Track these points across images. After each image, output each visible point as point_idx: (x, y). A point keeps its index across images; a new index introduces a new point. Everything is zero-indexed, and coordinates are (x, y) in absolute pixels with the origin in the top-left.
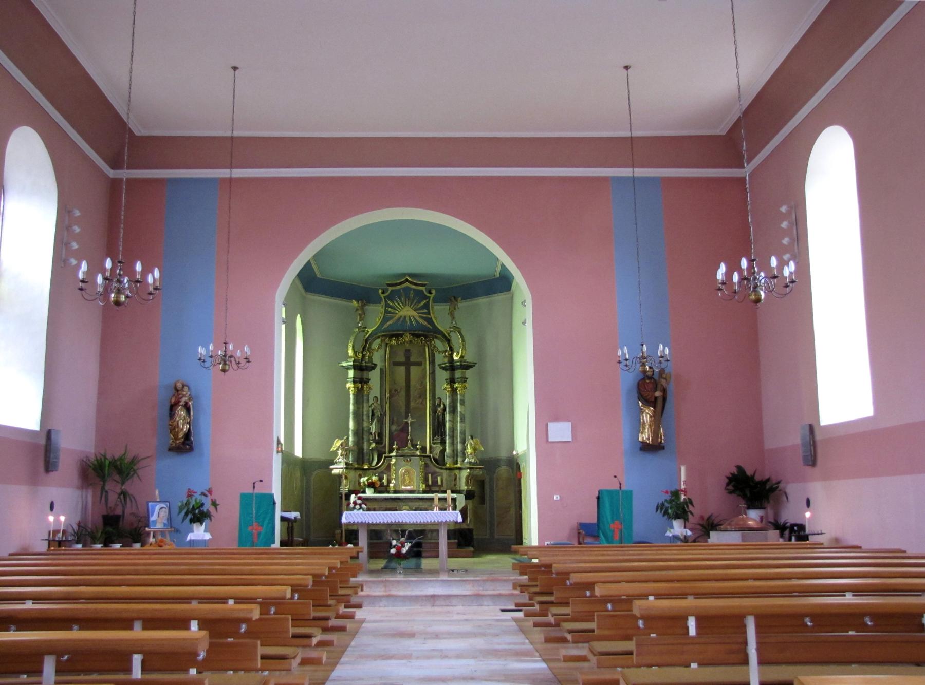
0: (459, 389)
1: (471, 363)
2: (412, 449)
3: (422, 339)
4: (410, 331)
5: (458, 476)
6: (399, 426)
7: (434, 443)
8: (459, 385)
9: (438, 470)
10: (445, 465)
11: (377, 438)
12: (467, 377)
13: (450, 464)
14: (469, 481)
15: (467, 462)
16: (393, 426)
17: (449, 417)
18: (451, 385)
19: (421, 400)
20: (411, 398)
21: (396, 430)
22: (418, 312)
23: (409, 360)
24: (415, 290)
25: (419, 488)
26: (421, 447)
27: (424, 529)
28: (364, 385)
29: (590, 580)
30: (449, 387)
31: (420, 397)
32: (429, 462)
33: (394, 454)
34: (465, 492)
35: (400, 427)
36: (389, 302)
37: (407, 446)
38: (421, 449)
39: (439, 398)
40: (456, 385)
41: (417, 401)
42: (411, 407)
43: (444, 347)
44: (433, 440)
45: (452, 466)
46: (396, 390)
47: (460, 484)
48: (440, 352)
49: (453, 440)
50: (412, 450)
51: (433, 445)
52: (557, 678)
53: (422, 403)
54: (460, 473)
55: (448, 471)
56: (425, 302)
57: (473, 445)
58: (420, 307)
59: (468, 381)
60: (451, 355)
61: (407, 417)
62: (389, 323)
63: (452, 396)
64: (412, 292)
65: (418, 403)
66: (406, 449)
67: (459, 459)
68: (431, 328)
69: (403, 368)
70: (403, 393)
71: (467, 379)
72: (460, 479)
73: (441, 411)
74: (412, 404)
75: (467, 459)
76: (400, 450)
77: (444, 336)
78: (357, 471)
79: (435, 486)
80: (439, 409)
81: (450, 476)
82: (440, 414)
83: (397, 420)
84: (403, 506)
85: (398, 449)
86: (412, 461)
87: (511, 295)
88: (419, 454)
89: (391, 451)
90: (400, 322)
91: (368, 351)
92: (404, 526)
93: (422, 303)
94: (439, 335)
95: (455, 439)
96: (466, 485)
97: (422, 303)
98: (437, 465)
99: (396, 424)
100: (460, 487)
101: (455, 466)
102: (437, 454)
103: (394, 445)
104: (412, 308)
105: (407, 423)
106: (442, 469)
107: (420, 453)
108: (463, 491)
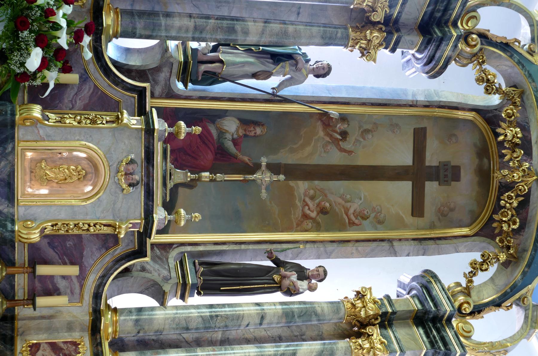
3: (515, 223)
11: (203, 68)
16: (238, 122)
18: (375, 316)
19: (313, 215)
21: (222, 133)
23: (431, 180)
28: (380, 30)
29: (14, 272)
30: (371, 313)
31: (323, 211)
32: (120, 250)
33: (159, 124)
35: (229, 145)
37: (176, 167)
39: (344, 298)
44: (190, 253)
46: (344, 134)
51: (174, 254)
53: (306, 216)
55: (87, 319)
61: (274, 168)
66: (169, 164)
77: (515, 289)
81: (70, 327)
82: (276, 277)
87: (319, 268)
89: (163, 113)
91: (481, 49)
103: (188, 125)
105: (255, 168)
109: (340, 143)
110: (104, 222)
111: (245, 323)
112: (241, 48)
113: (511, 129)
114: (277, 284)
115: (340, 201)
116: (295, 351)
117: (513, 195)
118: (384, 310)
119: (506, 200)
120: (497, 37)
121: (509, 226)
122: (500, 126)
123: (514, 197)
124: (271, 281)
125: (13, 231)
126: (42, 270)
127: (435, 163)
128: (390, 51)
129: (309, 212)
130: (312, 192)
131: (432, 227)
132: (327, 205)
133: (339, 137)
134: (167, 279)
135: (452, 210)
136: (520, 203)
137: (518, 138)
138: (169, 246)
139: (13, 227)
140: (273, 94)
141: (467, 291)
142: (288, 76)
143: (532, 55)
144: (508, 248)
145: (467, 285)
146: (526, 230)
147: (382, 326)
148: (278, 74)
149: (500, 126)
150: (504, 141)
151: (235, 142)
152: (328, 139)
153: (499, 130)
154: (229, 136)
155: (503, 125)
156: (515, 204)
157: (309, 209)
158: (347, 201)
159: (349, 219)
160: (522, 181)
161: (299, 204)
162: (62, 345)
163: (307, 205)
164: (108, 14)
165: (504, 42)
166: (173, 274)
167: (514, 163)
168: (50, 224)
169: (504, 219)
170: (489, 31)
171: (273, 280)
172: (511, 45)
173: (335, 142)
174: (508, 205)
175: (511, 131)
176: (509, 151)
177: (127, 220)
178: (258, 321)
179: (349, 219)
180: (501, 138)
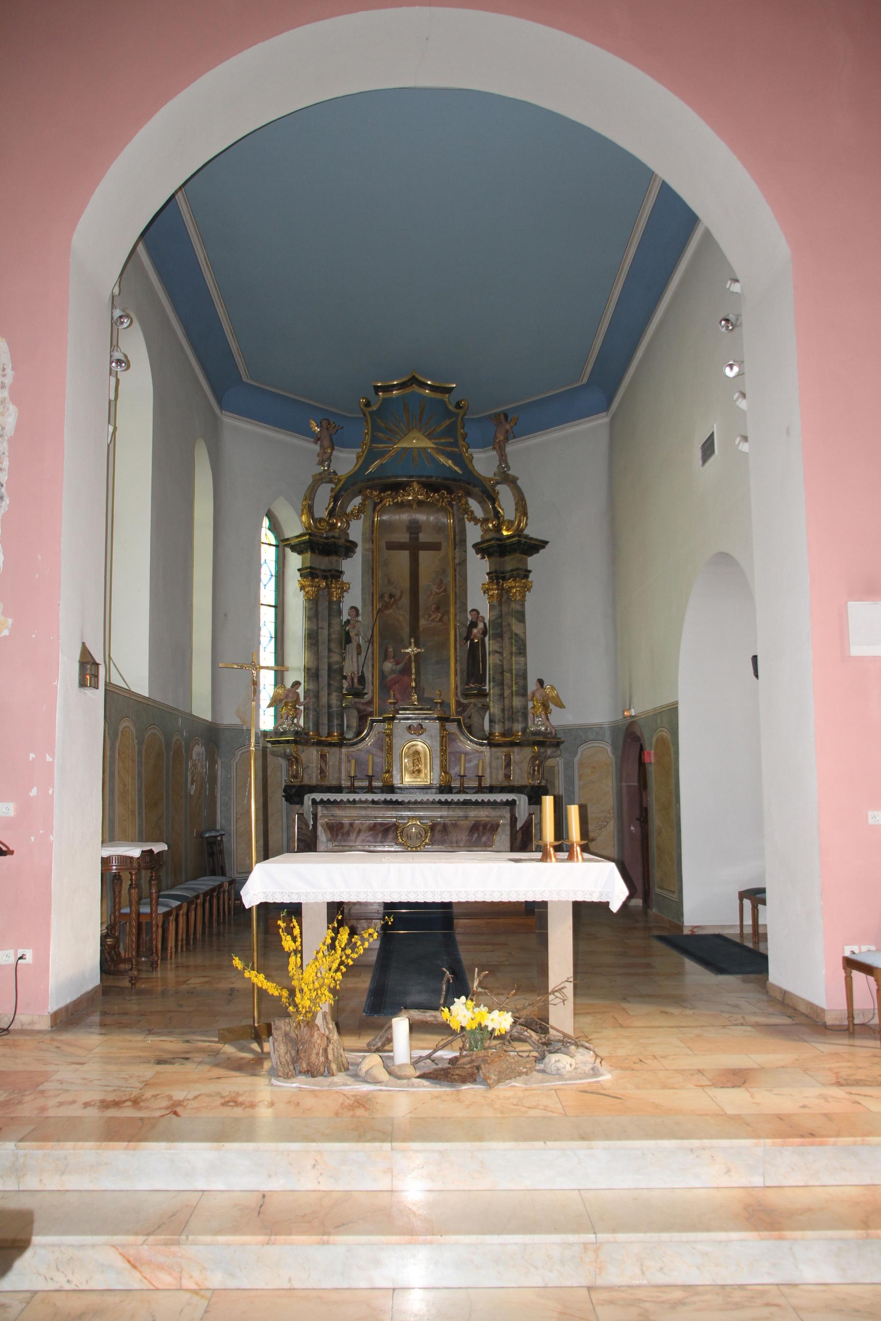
6: (397, 663)
19: (440, 615)
20: (421, 613)
21: (392, 671)
22: (433, 441)
28: (332, 583)
31: (438, 609)
35: (399, 667)
41: (433, 617)
53: (441, 620)
65: (433, 620)
69: (406, 554)
70: (406, 601)
71: (530, 571)
74: (423, 622)
83: (394, 651)
99: (392, 660)
109: (396, 598)
115: (431, 598)
125: (445, 786)
127: (407, 535)
130: (426, 616)
132: (434, 606)
133: (393, 599)
151: (397, 663)
152: (394, 607)
163: (434, 619)
173: (396, 602)
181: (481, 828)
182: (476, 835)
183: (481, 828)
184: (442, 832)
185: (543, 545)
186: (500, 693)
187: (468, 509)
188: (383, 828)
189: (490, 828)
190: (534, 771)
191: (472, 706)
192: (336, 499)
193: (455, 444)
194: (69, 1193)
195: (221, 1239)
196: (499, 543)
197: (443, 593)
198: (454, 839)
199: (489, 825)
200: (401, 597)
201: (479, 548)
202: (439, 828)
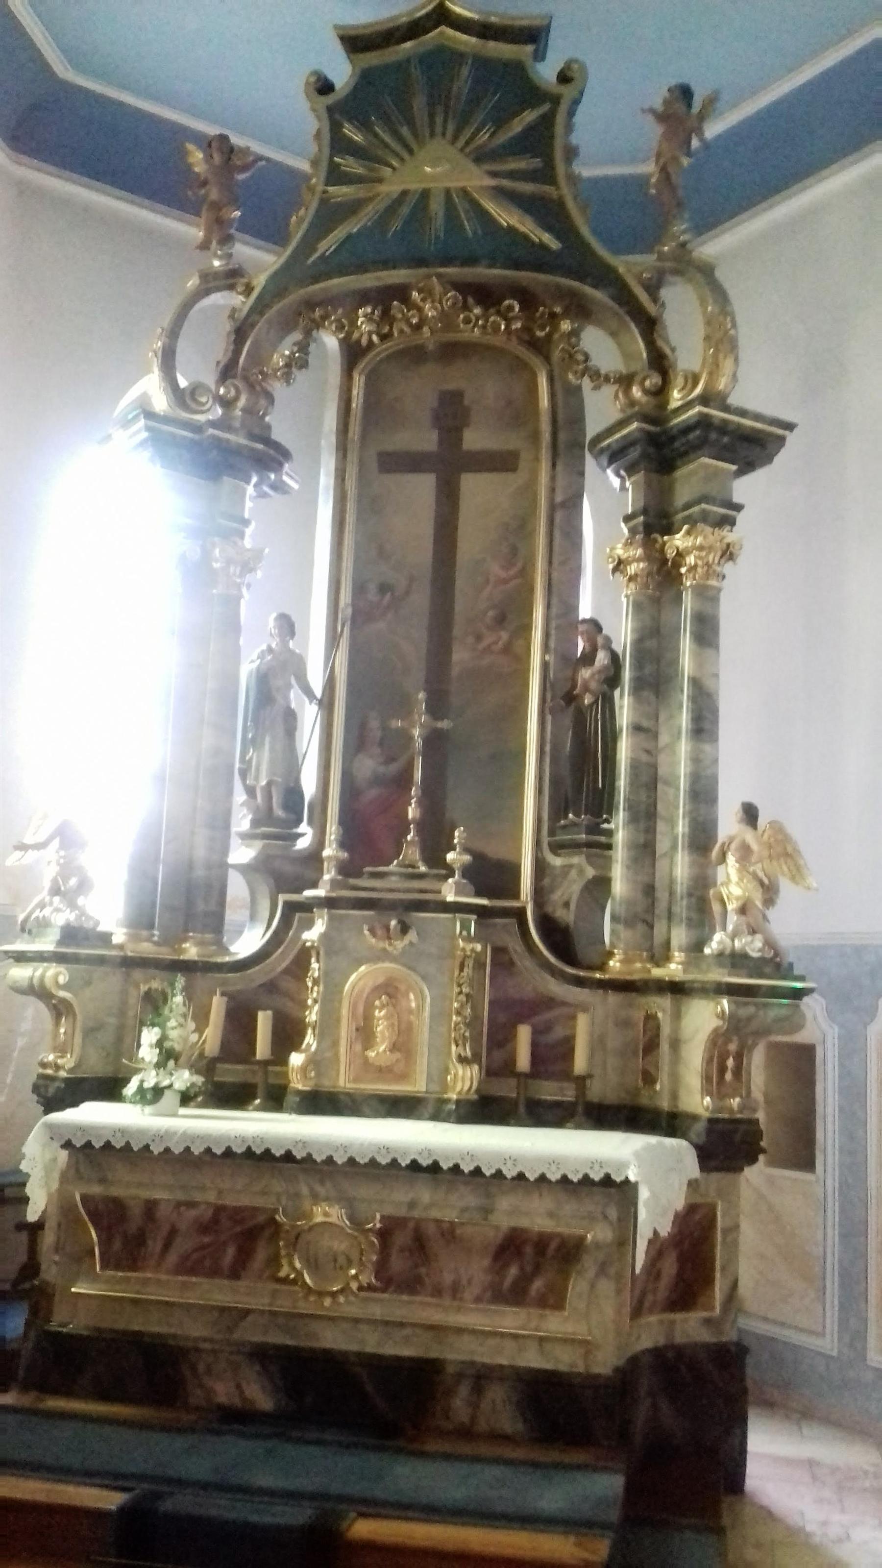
0: (691, 560)
1: (757, 417)
2: (423, 869)
3: (510, 308)
4: (447, 261)
5: (666, 1031)
7: (557, 848)
8: (689, 542)
9: (556, 988)
10: (602, 967)
12: (736, 499)
13: (626, 961)
14: (730, 1062)
15: (720, 955)
16: (360, 756)
17: (634, 709)
18: (648, 543)
19: (505, 636)
20: (457, 631)
22: (487, 167)
24: (483, 63)
25: (445, 1087)
26: (467, 858)
27: (433, 1355)
30: (639, 552)
31: (501, 620)
32: (515, 945)
34: (700, 1127)
36: (349, 131)
38: (468, 872)
40: (679, 541)
42: (455, 671)
43: (627, 356)
44: (552, 833)
45: (639, 970)
47: (675, 1078)
48: (599, 378)
49: (651, 831)
50: (421, 876)
52: (755, 876)
53: (507, 649)
54: (677, 1016)
55: (613, 998)
56: (530, 116)
57: (729, 319)
58: (503, 146)
59: (741, 518)
60: (661, 392)
62: (339, 234)
63: (656, 601)
64: (465, 71)
65: (488, 649)
66: (393, 867)
67: (680, 936)
68: (554, 245)
71: (738, 508)
72: (676, 1044)
73: (593, 685)
74: (460, 656)
75: (718, 936)
76: (359, 874)
78: (138, 974)
79: (549, 1076)
80: (585, 673)
82: (587, 700)
84: (316, 1198)
85: (347, 870)
86: (412, 936)
88: (450, 898)
90: (396, 225)
91: (245, 379)
92: (315, 1326)
93: (517, 126)
94: (595, 286)
95: (661, 826)
96: (707, 1090)
97: (517, 126)
98: (552, 959)
99: (377, 750)
100: (674, 1096)
101: (657, 972)
102: (567, 905)
103: (453, 848)
104: (462, 150)
106: (580, 982)
107: (457, 893)
108: (695, 1118)
109: (397, 594)
110: (457, 973)
111: (644, 758)
112: (249, 752)
113: (359, 323)
114: (596, 701)
115: (485, 593)
116: (690, 679)
117: (462, 316)
118: (641, 529)
119: (472, 325)
120: (226, 350)
121: (516, 318)
122: (358, 342)
123: (467, 313)
124: (595, 706)
125: (458, 1102)
126: (523, 1061)
127: (434, 436)
128: (247, 527)
129: (500, 643)
130: (470, 640)
131: (535, 436)
132: (491, 614)
133: (388, 596)
134: (581, 872)
135: (509, 403)
136: (479, 302)
137: (373, 313)
138: (540, 867)
139: (452, 1102)
140: (320, 703)
141: (625, 381)
142: (293, 681)
143: (252, 289)
144: (553, 316)
145: (614, 383)
146: (524, 284)
147: (669, 530)
148: (287, 698)
149: (358, 342)
150: (378, 334)
151: (390, 760)
152: (390, 616)
153: (364, 341)
154: (382, 769)
155: (356, 335)
156: (477, 311)
157: (496, 643)
158: (487, 581)
159: (515, 577)
160: (441, 303)
161: (486, 661)
162: (647, 1038)
163: (489, 646)
164: (184, 951)
165: (233, 337)
166: (576, 860)
167: (413, 316)
168: (454, 1047)
169: (503, 327)
170: (218, 363)
171: (591, 706)
172: (238, 324)
174: (480, 322)
175: (362, 323)
176: (395, 326)
177: (453, 938)
178: (642, 736)
179: (515, 577)
180: (375, 338)
181: (529, 1250)
182: (513, 1271)
183: (529, 1250)
184: (410, 1250)
185: (780, 432)
186: (642, 841)
187: (578, 345)
188: (238, 1229)
189: (558, 1249)
190: (722, 1070)
191: (573, 873)
192: (240, 334)
193: (547, 175)
194: (466, 1338)
195: (869, 1112)
196: (651, 428)
197: (518, 581)
198: (448, 1278)
199: (553, 1245)
200: (407, 593)
201: (602, 451)
202: (401, 1239)
